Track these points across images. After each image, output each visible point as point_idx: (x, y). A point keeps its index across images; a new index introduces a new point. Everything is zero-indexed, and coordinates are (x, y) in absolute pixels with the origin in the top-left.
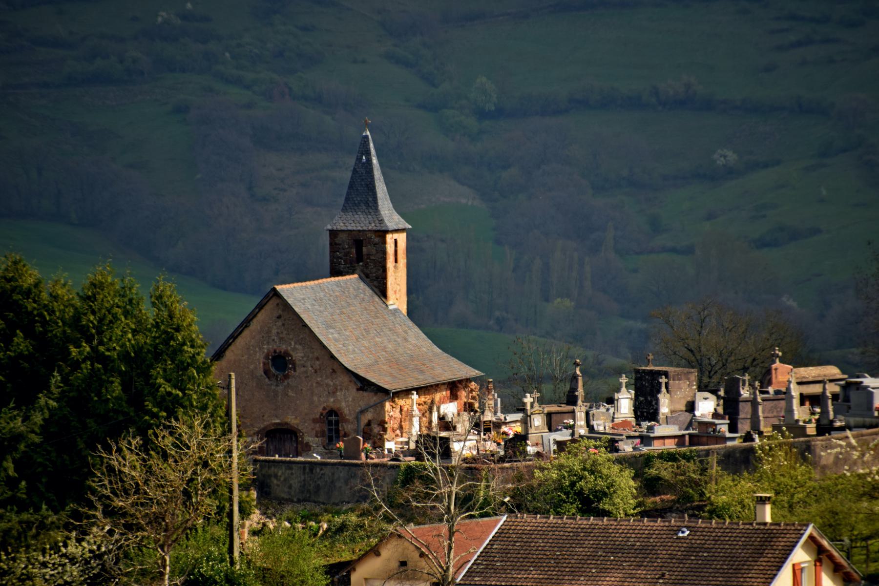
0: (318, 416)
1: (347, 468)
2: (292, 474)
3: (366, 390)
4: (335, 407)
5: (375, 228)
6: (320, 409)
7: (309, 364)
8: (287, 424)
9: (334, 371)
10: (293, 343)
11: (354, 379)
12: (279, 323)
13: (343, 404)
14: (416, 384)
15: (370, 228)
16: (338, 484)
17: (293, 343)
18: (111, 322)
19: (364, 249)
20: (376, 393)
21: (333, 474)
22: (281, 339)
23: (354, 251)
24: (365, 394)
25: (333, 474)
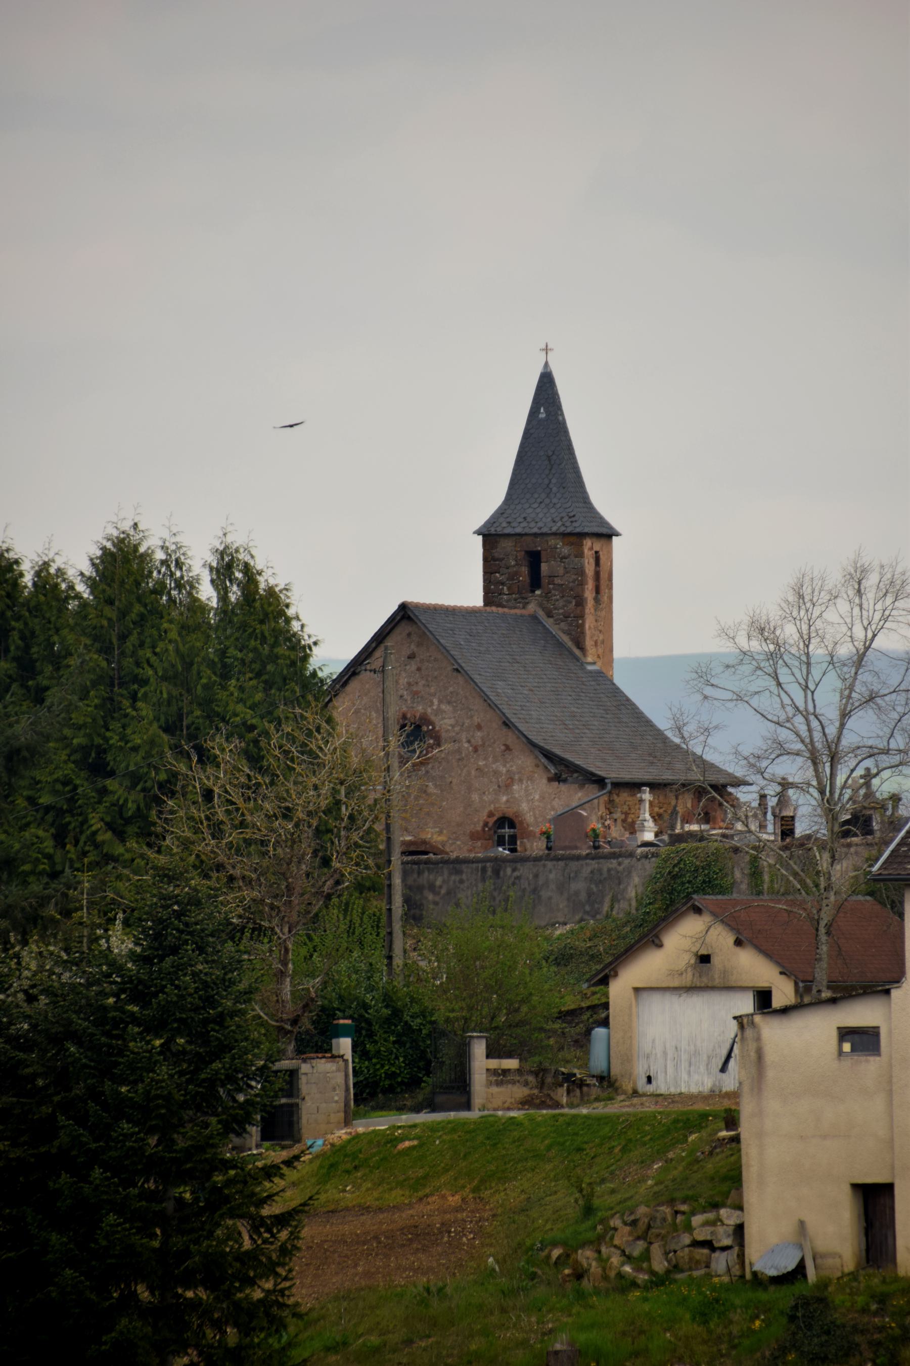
0: (479, 828)
1: (561, 863)
2: (461, 881)
3: (565, 781)
4: (510, 813)
5: (562, 529)
6: (484, 815)
7: (464, 736)
8: (424, 842)
9: (508, 748)
10: (436, 702)
11: (544, 760)
12: (413, 667)
13: (524, 806)
14: (647, 777)
15: (554, 529)
16: (545, 894)
17: (436, 702)
18: (142, 617)
19: (544, 567)
20: (582, 786)
21: (536, 876)
22: (415, 694)
23: (525, 570)
24: (563, 787)
25: (536, 876)
